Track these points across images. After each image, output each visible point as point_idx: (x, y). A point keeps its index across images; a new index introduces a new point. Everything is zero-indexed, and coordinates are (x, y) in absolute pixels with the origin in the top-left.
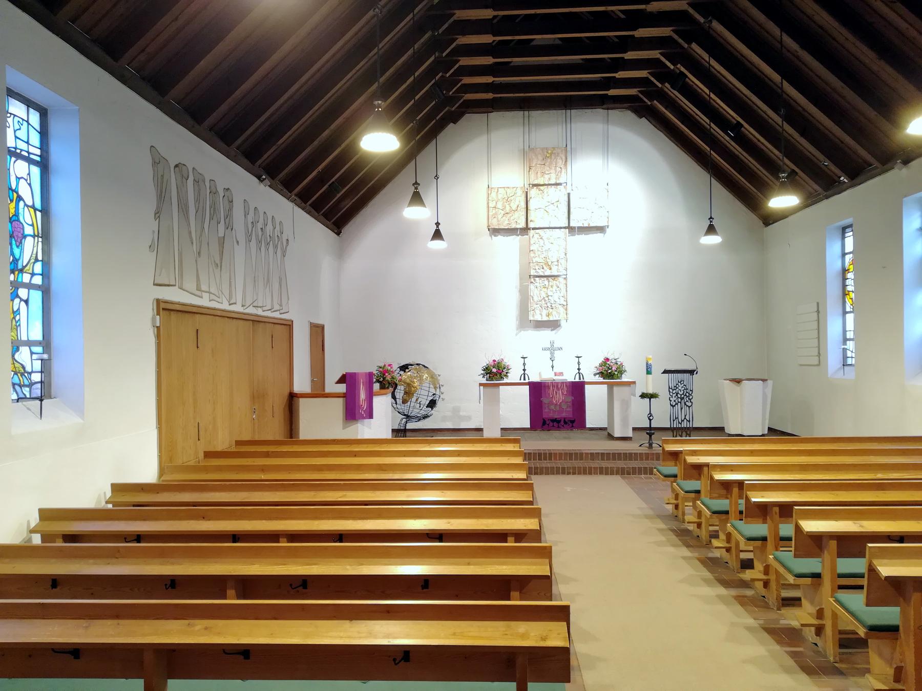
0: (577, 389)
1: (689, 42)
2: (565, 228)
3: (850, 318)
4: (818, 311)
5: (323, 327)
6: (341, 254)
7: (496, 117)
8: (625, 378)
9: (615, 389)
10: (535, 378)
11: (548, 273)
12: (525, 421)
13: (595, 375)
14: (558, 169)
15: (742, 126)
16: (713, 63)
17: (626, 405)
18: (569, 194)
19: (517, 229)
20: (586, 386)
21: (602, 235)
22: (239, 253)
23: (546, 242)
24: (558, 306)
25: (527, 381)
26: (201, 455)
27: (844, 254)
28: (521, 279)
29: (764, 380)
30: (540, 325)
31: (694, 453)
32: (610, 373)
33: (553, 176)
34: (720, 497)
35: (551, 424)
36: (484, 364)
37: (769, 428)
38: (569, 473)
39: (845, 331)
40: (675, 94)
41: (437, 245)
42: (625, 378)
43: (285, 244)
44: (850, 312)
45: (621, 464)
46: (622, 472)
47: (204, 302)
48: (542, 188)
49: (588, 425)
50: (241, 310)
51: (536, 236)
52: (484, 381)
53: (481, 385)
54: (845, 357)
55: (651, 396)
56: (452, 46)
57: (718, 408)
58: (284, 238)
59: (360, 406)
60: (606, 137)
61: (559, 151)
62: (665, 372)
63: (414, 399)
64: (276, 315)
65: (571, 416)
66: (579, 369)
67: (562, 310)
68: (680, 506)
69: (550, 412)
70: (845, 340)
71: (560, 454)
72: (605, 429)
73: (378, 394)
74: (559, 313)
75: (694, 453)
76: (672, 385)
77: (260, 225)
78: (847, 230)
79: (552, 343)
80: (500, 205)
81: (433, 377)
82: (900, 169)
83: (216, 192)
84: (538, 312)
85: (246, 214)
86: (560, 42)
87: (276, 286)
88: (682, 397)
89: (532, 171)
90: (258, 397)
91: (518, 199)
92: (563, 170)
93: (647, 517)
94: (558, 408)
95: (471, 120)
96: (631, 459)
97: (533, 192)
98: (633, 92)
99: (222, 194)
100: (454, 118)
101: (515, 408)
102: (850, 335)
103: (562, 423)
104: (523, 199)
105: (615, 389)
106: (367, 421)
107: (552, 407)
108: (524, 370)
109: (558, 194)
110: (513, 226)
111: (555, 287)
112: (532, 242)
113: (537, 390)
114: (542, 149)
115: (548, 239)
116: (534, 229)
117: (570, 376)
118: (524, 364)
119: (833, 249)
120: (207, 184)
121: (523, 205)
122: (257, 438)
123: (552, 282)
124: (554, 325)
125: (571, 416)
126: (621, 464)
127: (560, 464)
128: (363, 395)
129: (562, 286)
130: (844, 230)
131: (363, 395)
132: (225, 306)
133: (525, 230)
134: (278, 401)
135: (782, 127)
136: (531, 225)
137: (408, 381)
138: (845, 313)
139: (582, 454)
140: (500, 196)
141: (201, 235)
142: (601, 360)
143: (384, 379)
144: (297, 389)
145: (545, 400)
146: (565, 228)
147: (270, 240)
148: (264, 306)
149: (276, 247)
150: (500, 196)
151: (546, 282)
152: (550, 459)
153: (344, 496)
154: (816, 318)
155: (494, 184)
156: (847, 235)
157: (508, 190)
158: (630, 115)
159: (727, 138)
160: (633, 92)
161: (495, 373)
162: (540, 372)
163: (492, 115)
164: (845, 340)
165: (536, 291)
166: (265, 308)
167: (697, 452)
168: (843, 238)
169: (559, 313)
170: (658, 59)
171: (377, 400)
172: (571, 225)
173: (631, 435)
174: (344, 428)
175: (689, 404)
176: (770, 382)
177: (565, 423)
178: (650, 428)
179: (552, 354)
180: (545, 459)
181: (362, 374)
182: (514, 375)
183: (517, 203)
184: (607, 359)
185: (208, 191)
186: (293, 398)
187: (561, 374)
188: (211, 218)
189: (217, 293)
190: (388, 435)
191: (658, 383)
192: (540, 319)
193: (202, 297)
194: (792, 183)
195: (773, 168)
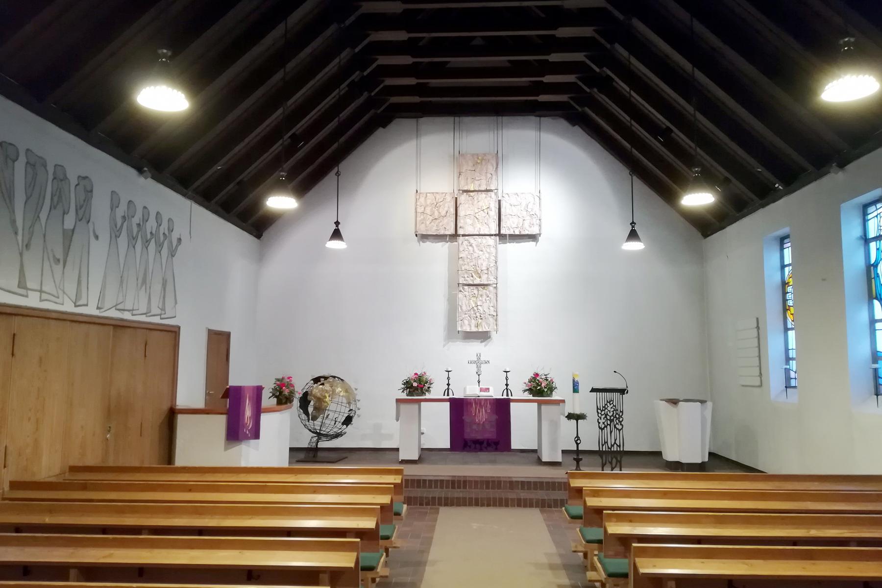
0: (502, 407)
1: (611, 43)
2: (495, 235)
3: (792, 334)
4: (758, 327)
5: (227, 335)
6: (260, 257)
7: (426, 122)
8: (555, 396)
9: (543, 407)
10: (458, 395)
11: (477, 281)
12: (443, 440)
13: (525, 391)
14: (489, 176)
15: (672, 131)
16: (633, 60)
17: (555, 425)
18: (500, 201)
19: (446, 235)
20: (512, 404)
21: (534, 243)
22: (99, 249)
25: (451, 396)
26: (6, 487)
27: (783, 267)
28: (449, 287)
29: (703, 402)
30: (469, 336)
31: (597, 493)
32: (539, 389)
33: (484, 182)
34: (616, 555)
35: (473, 446)
36: (405, 377)
37: (710, 454)
38: (483, 505)
39: (787, 350)
40: (603, 99)
41: (335, 245)
42: (555, 396)
43: (175, 243)
44: (792, 329)
45: (541, 494)
46: (543, 505)
47: (32, 301)
48: (472, 194)
49: (514, 446)
50: (96, 313)
51: (465, 243)
52: (404, 396)
53: (399, 401)
54: (788, 379)
55: (576, 417)
56: (365, 42)
57: (655, 431)
58: (175, 236)
59: (244, 425)
62: (593, 390)
64: (156, 320)
66: (507, 385)
67: (491, 320)
68: (589, 556)
69: (471, 433)
70: (788, 359)
71: (476, 482)
72: (535, 451)
73: (269, 410)
75: (597, 493)
76: (601, 405)
77: (136, 220)
78: (786, 241)
79: (479, 356)
80: (428, 211)
81: (347, 390)
82: (837, 173)
83: (65, 178)
84: (466, 322)
85: (114, 206)
86: (508, 65)
87: (157, 288)
88: (612, 418)
89: (462, 177)
90: (115, 412)
92: (494, 177)
93: (552, 567)
95: (400, 125)
96: (554, 489)
97: (463, 198)
98: (563, 98)
99: (74, 181)
100: (383, 121)
101: (438, 432)
102: (792, 354)
104: (453, 203)
106: (253, 442)
107: (475, 427)
108: (448, 385)
109: (489, 201)
110: (442, 232)
111: (485, 297)
112: (461, 249)
113: (459, 408)
114: (473, 155)
115: (477, 246)
116: (463, 235)
117: (496, 393)
118: (448, 378)
119: (772, 260)
120: (51, 170)
121: (453, 211)
122: (111, 463)
124: (484, 336)
125: (494, 437)
126: (541, 494)
127: (473, 493)
128: (248, 412)
129: (492, 296)
130: (782, 240)
131: (248, 412)
132: (68, 307)
133: (455, 236)
134: (153, 418)
135: (694, 116)
136: (460, 232)
137: (318, 395)
138: (786, 329)
139: (499, 482)
140: (429, 202)
141: (33, 225)
143: (281, 393)
144: (181, 402)
145: (466, 418)
146: (495, 235)
147: (165, 242)
148: (137, 308)
149: (160, 246)
150: (429, 202)
151: (475, 291)
152: (465, 487)
153: (110, 556)
154: (756, 335)
155: (424, 189)
156: (785, 246)
157: (438, 197)
158: (563, 123)
159: (657, 143)
160: (563, 98)
161: (416, 388)
162: (467, 388)
164: (788, 359)
165: (465, 299)
166: (135, 312)
167: (613, 489)
168: (782, 249)
169: (489, 325)
170: (583, 63)
171: (264, 418)
172: (503, 232)
173: (560, 459)
174: (226, 449)
175: (619, 427)
176: (709, 404)
177: (489, 445)
178: (578, 452)
179: (478, 367)
180: (459, 487)
181: (249, 387)
182: (437, 391)
183: (446, 209)
184: (537, 375)
185: (51, 177)
186: (172, 414)
187: (487, 390)
188: (53, 207)
189: (55, 293)
190: (282, 460)
191: (585, 402)
192: (468, 330)
193: (27, 296)
194: (707, 179)
195: (689, 160)
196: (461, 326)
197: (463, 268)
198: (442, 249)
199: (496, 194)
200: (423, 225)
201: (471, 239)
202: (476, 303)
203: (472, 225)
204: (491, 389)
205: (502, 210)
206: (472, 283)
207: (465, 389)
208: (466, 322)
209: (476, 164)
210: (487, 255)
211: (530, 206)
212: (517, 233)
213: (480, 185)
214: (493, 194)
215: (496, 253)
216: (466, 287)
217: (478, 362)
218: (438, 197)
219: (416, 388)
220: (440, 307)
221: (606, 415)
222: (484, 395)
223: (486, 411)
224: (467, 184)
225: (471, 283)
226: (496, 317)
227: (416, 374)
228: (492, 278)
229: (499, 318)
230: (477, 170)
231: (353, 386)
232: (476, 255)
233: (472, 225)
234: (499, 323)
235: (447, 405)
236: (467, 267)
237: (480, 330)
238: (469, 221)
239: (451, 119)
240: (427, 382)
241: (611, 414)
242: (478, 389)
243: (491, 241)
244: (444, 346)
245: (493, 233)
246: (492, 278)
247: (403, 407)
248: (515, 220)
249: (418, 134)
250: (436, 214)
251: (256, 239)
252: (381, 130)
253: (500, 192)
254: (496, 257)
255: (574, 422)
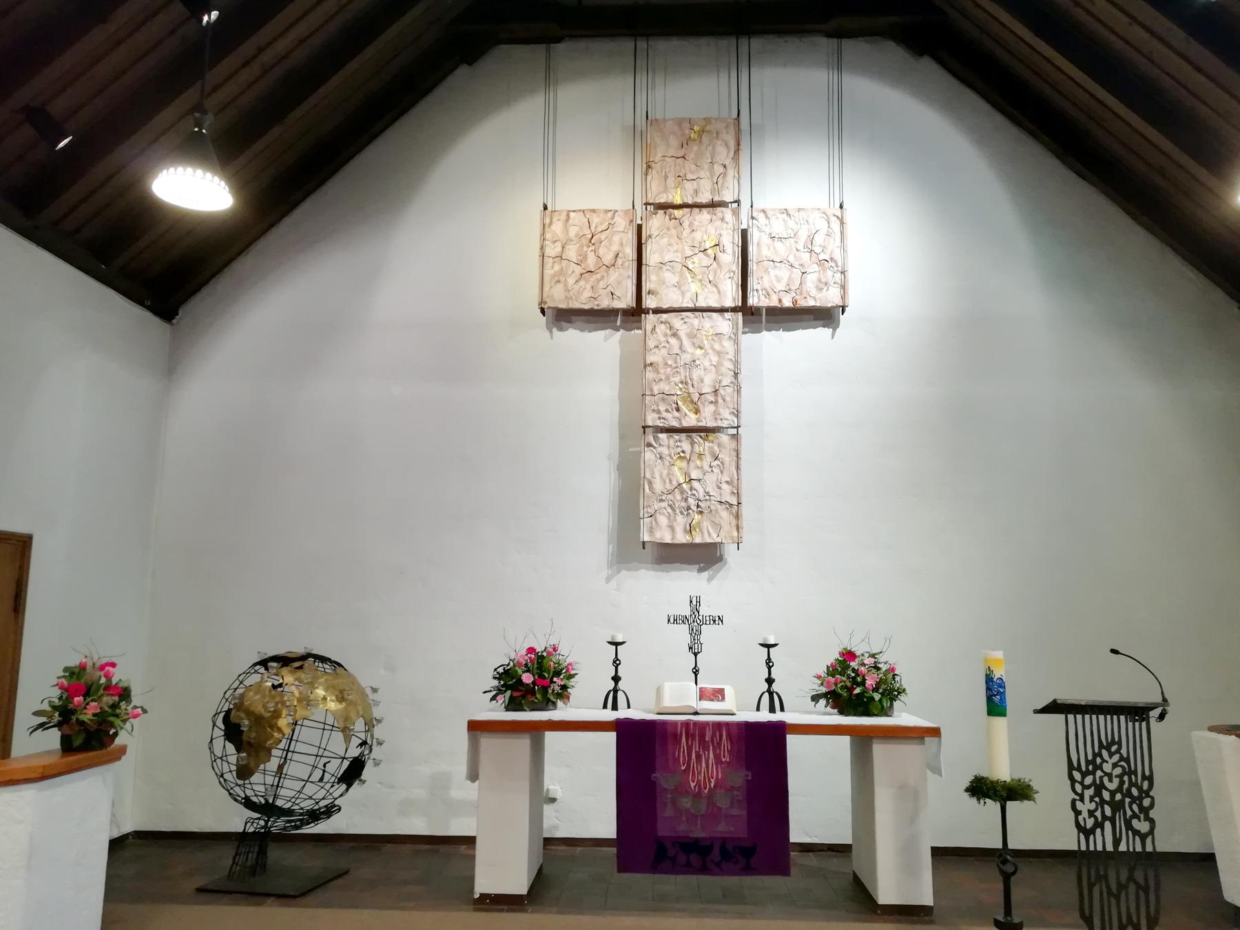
0: (762, 747)
2: (734, 310)
6: (171, 366)
8: (902, 716)
9: (880, 750)
11: (691, 420)
13: (815, 698)
14: (718, 169)
17: (911, 797)
18: (744, 234)
20: (791, 740)
23: (686, 343)
24: (715, 506)
25: (623, 713)
28: (622, 437)
30: (673, 555)
32: (856, 690)
35: (682, 859)
36: (501, 659)
42: (902, 716)
48: (677, 213)
51: (661, 329)
53: (475, 727)
60: (838, 99)
61: (721, 126)
62: (1054, 708)
63: (273, 764)
65: (743, 833)
66: (770, 681)
67: (725, 516)
69: (676, 819)
74: (718, 527)
76: (1082, 755)
79: (695, 604)
80: (572, 253)
84: (663, 520)
89: (653, 173)
91: (616, 239)
92: (731, 172)
94: (703, 807)
97: (656, 224)
101: (584, 792)
103: (716, 854)
104: (631, 237)
105: (880, 750)
107: (686, 803)
108: (616, 679)
109: (717, 231)
110: (605, 303)
111: (708, 458)
112: (651, 343)
113: (643, 748)
114: (680, 122)
115: (691, 336)
116: (657, 311)
117: (741, 706)
118: (616, 663)
121: (630, 252)
123: (702, 446)
124: (705, 556)
125: (743, 833)
133: (636, 313)
136: (649, 302)
137: (259, 709)
140: (573, 232)
142: (832, 656)
145: (665, 781)
146: (734, 310)
150: (573, 232)
151: (686, 446)
158: (893, 52)
161: (532, 684)
163: (560, 47)
169: (718, 527)
175: (1143, 827)
177: (726, 855)
179: (695, 634)
182: (582, 703)
183: (615, 248)
184: (849, 655)
187: (719, 694)
192: (668, 540)
196: (651, 531)
197: (656, 390)
198: (605, 344)
199: (736, 213)
200: (560, 286)
201: (674, 319)
202: (686, 474)
203: (678, 286)
204: (729, 692)
205: (752, 250)
206: (673, 425)
207: (659, 691)
208: (663, 520)
209: (685, 143)
210: (715, 359)
211: (819, 239)
212: (787, 303)
213: (696, 192)
214: (727, 213)
215: (737, 352)
216: (663, 436)
217: (694, 620)
218: (595, 219)
219: (532, 684)
220: (597, 486)
221: (1099, 788)
222: (711, 711)
223: (717, 757)
224: (666, 190)
225: (675, 424)
226: (735, 509)
227: (531, 650)
228: (726, 413)
229: (745, 509)
230: (691, 156)
231: (365, 681)
232: (686, 358)
233: (678, 286)
234: (745, 523)
235: (609, 739)
236: (665, 387)
237: (698, 540)
238: (670, 277)
239: (628, 44)
240: (558, 673)
241: (1113, 786)
242: (693, 690)
243: (724, 324)
244: (608, 579)
245: (729, 303)
246: (726, 413)
247: (488, 742)
248: (784, 272)
249: (549, 79)
250: (591, 262)
251: (156, 320)
252: (463, 70)
253: (745, 205)
254: (736, 363)
255: (993, 807)
